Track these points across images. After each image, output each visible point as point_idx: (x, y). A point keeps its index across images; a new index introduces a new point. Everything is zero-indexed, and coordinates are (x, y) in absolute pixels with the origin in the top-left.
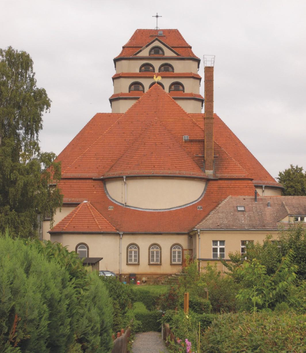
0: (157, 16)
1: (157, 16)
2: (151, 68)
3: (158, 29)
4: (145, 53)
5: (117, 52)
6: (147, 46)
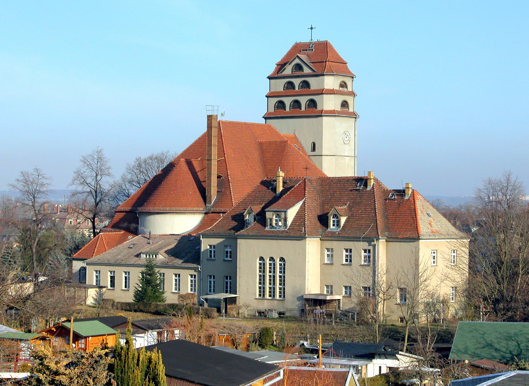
0: (312, 28)
1: (312, 28)
3: (312, 41)
4: (288, 70)
5: (271, 69)
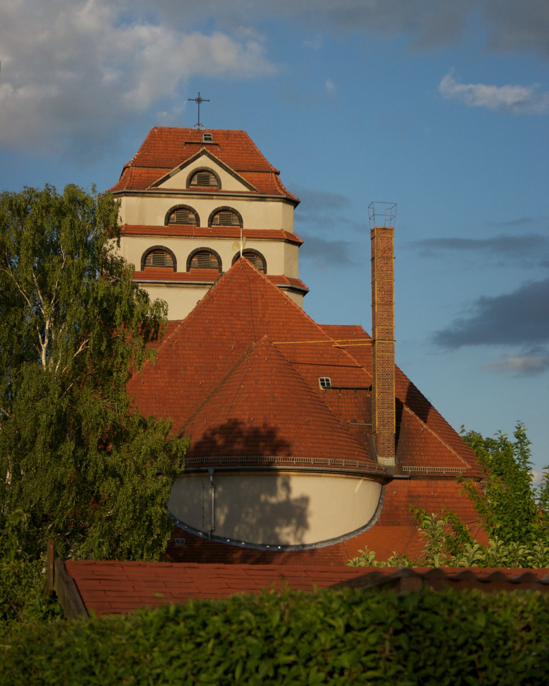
0: (199, 100)
2: (192, 216)
6: (182, 168)
